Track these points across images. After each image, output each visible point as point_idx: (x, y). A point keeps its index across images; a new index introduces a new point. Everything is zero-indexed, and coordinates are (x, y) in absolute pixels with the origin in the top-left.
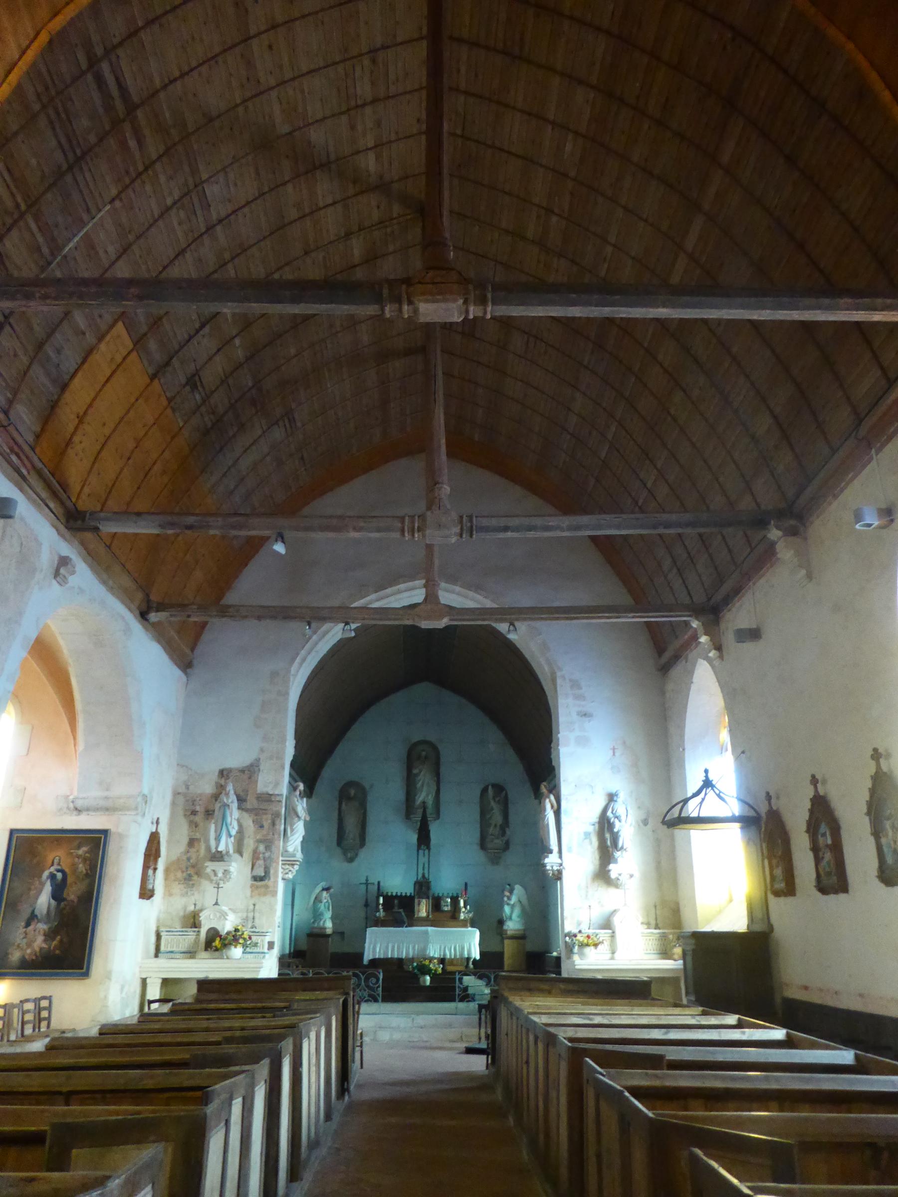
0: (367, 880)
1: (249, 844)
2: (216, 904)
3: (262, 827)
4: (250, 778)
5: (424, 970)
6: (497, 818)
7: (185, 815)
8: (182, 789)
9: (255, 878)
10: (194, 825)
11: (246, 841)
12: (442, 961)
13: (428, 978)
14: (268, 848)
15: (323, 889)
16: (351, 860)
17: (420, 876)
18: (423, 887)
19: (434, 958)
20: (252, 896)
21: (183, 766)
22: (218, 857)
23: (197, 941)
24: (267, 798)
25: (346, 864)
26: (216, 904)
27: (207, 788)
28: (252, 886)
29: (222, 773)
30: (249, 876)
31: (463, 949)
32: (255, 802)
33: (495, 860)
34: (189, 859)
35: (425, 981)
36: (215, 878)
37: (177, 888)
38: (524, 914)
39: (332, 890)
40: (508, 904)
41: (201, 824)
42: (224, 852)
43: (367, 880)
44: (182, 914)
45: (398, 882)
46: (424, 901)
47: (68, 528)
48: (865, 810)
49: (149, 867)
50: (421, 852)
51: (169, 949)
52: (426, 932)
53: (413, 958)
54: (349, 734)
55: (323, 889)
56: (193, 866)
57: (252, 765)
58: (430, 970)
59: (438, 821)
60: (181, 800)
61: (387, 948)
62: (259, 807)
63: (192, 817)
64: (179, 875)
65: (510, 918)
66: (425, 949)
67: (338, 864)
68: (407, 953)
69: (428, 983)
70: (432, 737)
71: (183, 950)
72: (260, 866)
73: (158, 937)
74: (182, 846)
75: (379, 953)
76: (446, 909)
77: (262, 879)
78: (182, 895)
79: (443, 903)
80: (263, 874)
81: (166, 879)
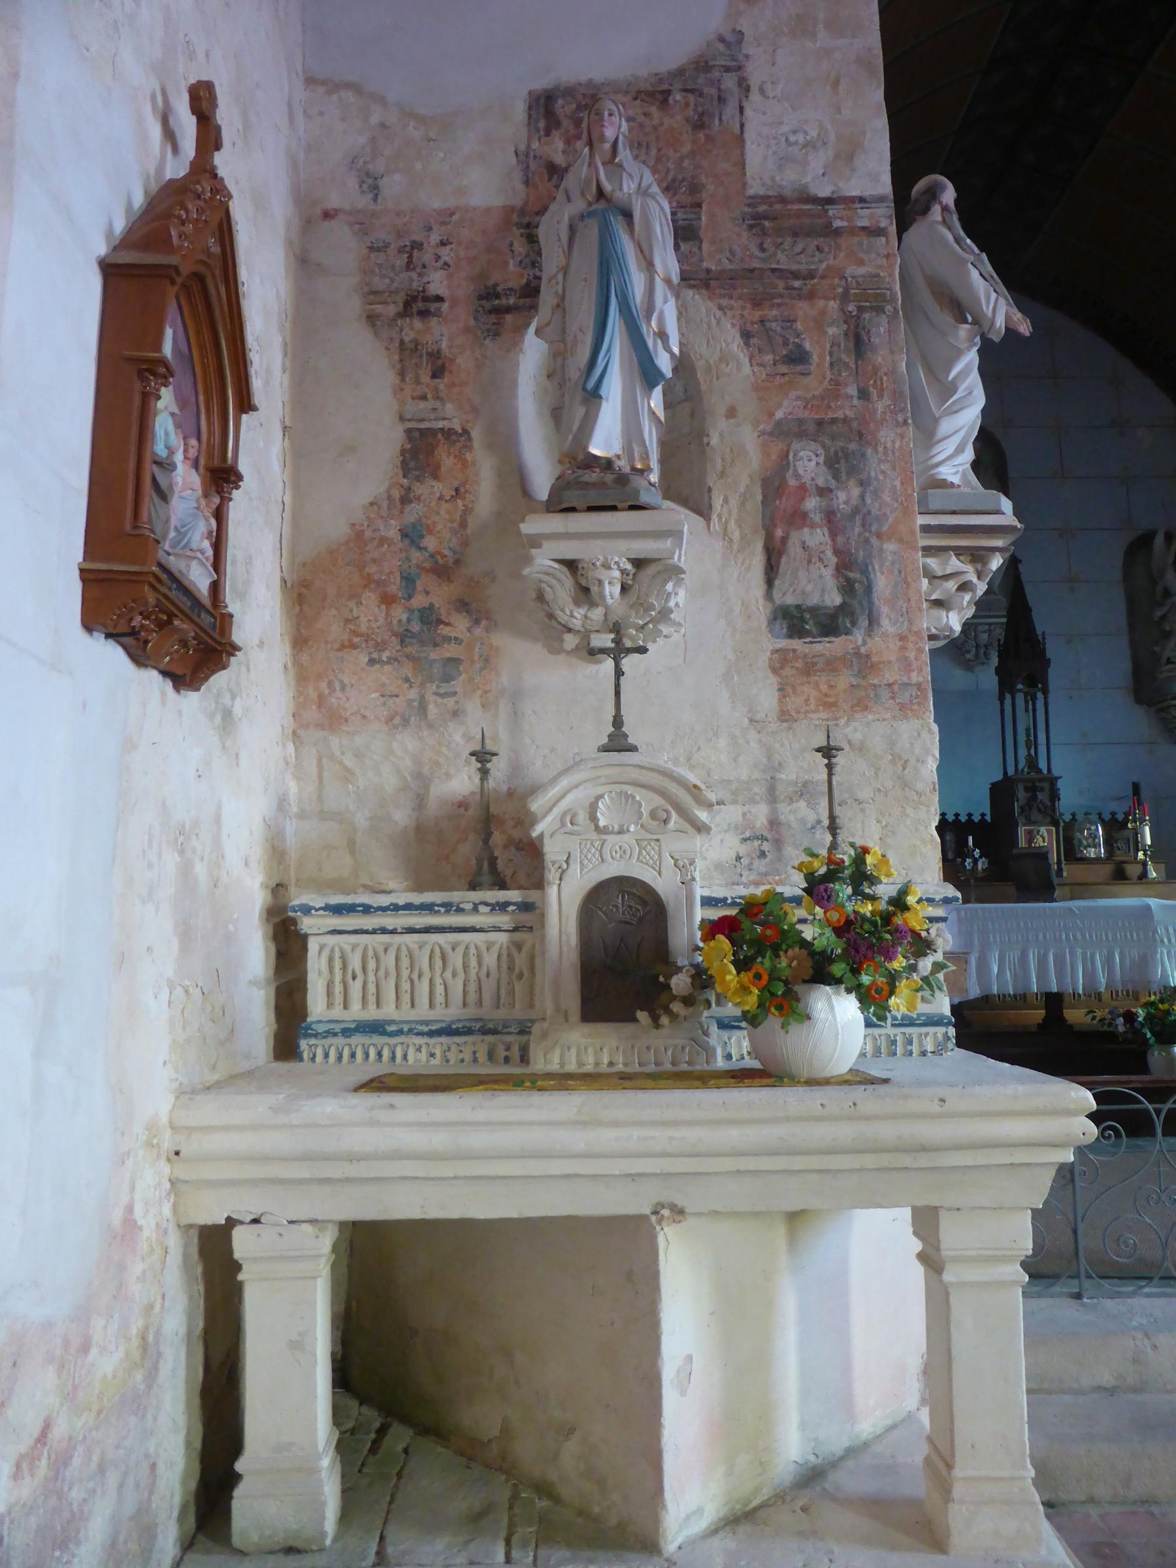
1: (739, 446)
2: (618, 743)
3: (798, 358)
4: (699, 124)
7: (372, 319)
8: (344, 194)
9: (794, 621)
10: (425, 365)
11: (718, 434)
14: (842, 464)
20: (785, 716)
21: (334, 86)
22: (591, 487)
23: (521, 963)
24: (800, 218)
26: (618, 743)
27: (478, 180)
28: (780, 662)
29: (545, 107)
30: (761, 610)
32: (743, 242)
34: (412, 535)
36: (577, 616)
37: (364, 686)
41: (464, 362)
42: (623, 464)
44: (402, 816)
46: (1043, 830)
47: (265, 915)
48: (1060, 784)
49: (153, 371)
51: (356, 1012)
56: (442, 571)
57: (702, 65)
60: (342, 248)
62: (763, 260)
63: (412, 329)
64: (369, 613)
66: (1145, 962)
68: (1090, 975)
71: (454, 1013)
72: (811, 556)
73: (287, 941)
74: (372, 474)
76: (1091, 853)
77: (830, 624)
78: (397, 721)
80: (834, 599)
81: (299, 641)
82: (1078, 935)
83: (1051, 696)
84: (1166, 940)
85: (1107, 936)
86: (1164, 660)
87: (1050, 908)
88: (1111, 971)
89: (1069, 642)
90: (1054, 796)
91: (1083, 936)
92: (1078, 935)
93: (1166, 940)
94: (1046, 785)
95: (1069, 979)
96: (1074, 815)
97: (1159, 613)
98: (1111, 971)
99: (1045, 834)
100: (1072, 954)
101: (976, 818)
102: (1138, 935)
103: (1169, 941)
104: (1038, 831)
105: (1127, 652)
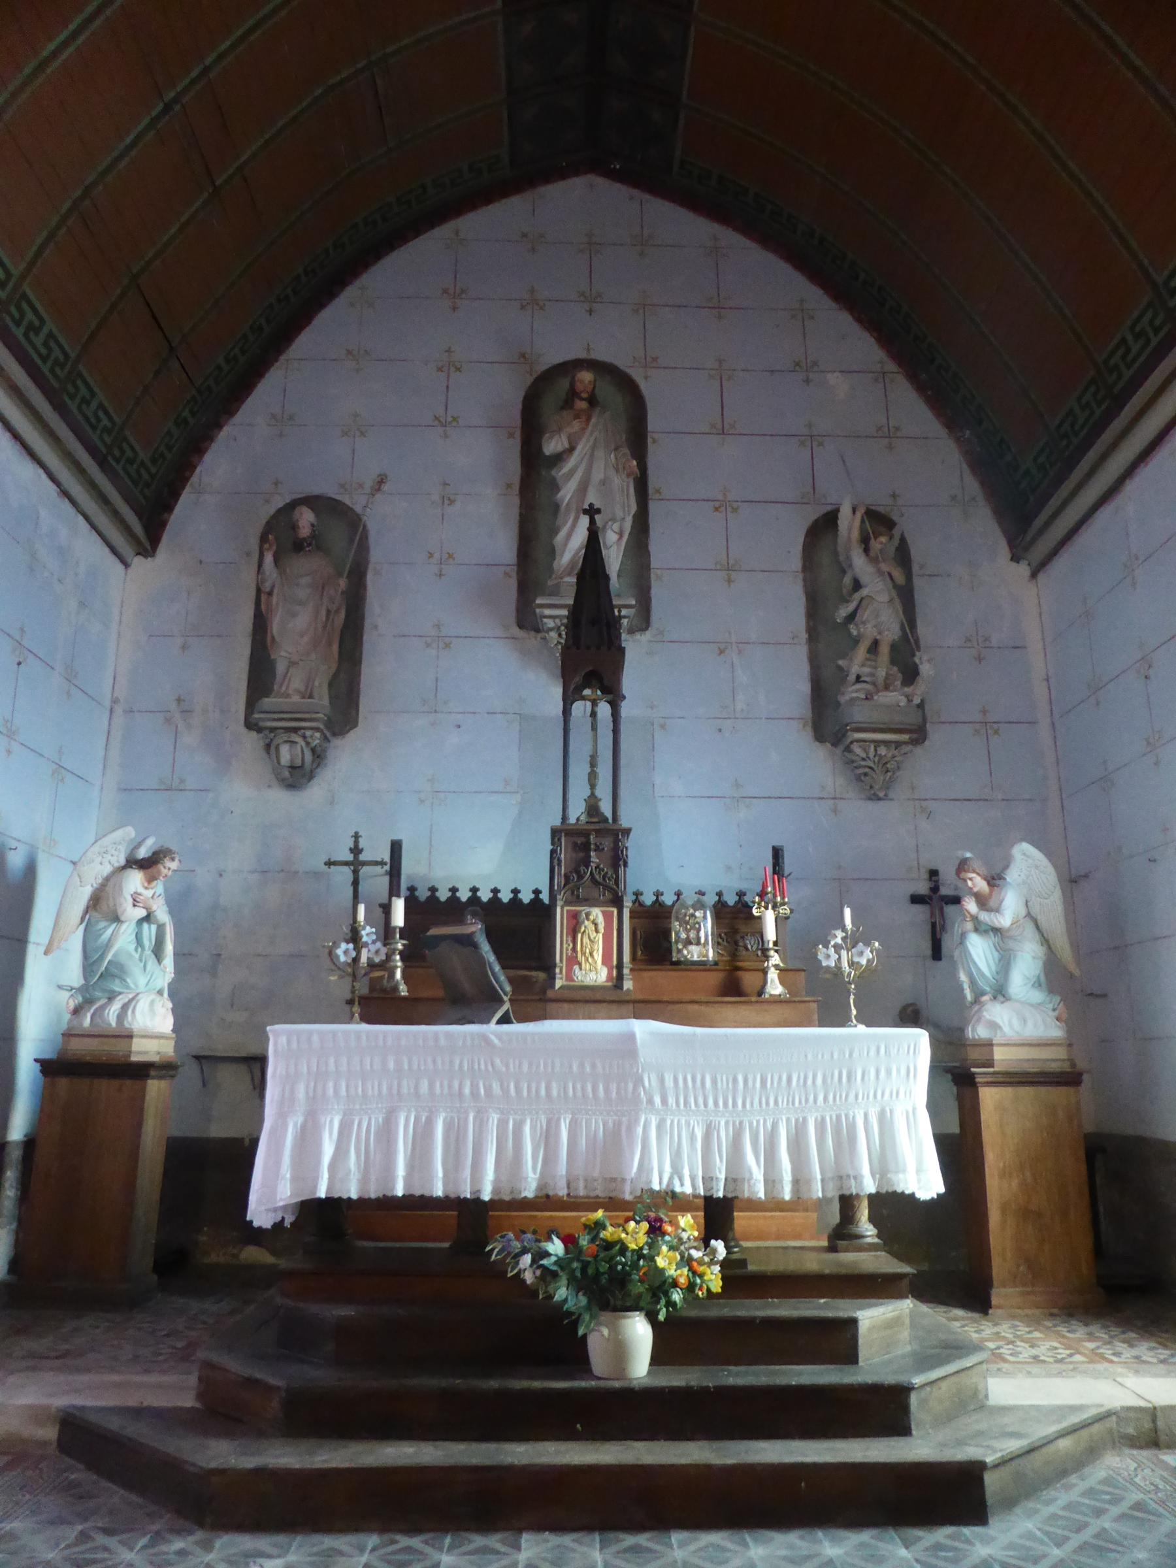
0: (356, 850)
5: (614, 1283)
6: (880, 619)
12: (718, 1215)
13: (639, 1331)
15: (132, 863)
16: (296, 777)
17: (577, 811)
18: (591, 852)
19: (679, 1203)
25: (280, 797)
31: (845, 1139)
33: (872, 779)
35: (620, 1351)
38: (1055, 977)
39: (170, 866)
40: (980, 928)
43: (356, 850)
45: (489, 852)
46: (597, 913)
50: (580, 709)
52: (627, 1047)
53: (545, 1201)
54: (304, 342)
55: (132, 863)
58: (661, 1286)
59: (648, 635)
61: (386, 1134)
65: (1000, 992)
66: (615, 1142)
67: (247, 795)
68: (510, 1163)
69: (640, 1367)
70: (614, 349)
75: (338, 1174)
76: (694, 953)
79: (678, 931)
82: (496, 1087)
83: (625, 709)
84: (657, 1100)
85: (548, 1089)
86: (852, 678)
87: (448, 1035)
88: (549, 1160)
89: (721, 652)
90: (618, 859)
91: (505, 1091)
92: (496, 1087)
93: (657, 1100)
94: (607, 843)
95: (467, 1173)
96: (678, 894)
97: (843, 612)
98: (549, 1160)
99: (601, 920)
100: (481, 1124)
101: (526, 897)
102: (607, 1090)
103: (664, 1102)
104: (588, 915)
105: (805, 668)
